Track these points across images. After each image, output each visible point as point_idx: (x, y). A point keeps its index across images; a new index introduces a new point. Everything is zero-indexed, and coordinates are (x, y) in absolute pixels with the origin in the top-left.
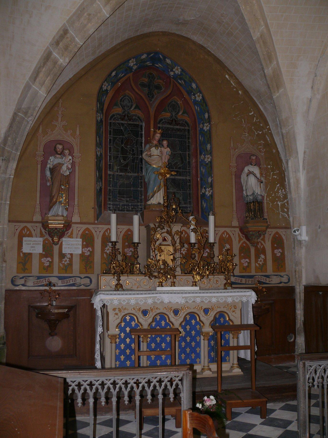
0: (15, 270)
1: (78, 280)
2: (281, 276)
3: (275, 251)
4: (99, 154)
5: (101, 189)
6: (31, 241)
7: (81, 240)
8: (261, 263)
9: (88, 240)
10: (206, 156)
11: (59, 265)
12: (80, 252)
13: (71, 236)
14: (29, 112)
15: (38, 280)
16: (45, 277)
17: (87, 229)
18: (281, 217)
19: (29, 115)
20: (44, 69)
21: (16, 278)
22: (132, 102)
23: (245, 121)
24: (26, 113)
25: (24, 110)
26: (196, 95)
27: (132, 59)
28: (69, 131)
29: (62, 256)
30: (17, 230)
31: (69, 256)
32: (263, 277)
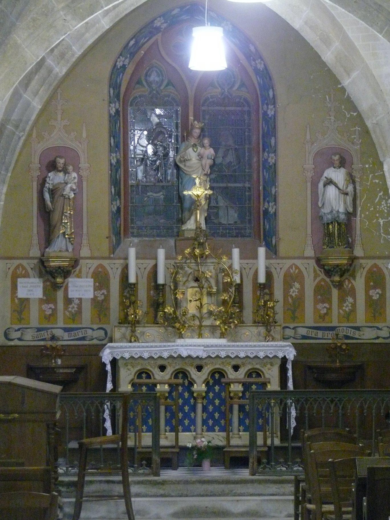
0: (9, 321)
1: (90, 332)
2: (378, 328)
3: (371, 291)
4: (114, 162)
5: (119, 209)
6: (28, 283)
7: (92, 280)
8: (347, 309)
9: (101, 280)
10: (270, 155)
11: (64, 313)
12: (92, 296)
13: (79, 276)
14: (21, 125)
15: (38, 333)
16: (46, 329)
17: (101, 266)
18: (382, 241)
19: (20, 128)
20: (37, 76)
21: (11, 330)
22: (162, 75)
23: (330, 98)
24: (17, 127)
25: (13, 122)
26: (257, 62)
27: (159, 19)
28: (72, 134)
29: (68, 301)
30: (9, 268)
31: (77, 302)
32: (350, 329)
